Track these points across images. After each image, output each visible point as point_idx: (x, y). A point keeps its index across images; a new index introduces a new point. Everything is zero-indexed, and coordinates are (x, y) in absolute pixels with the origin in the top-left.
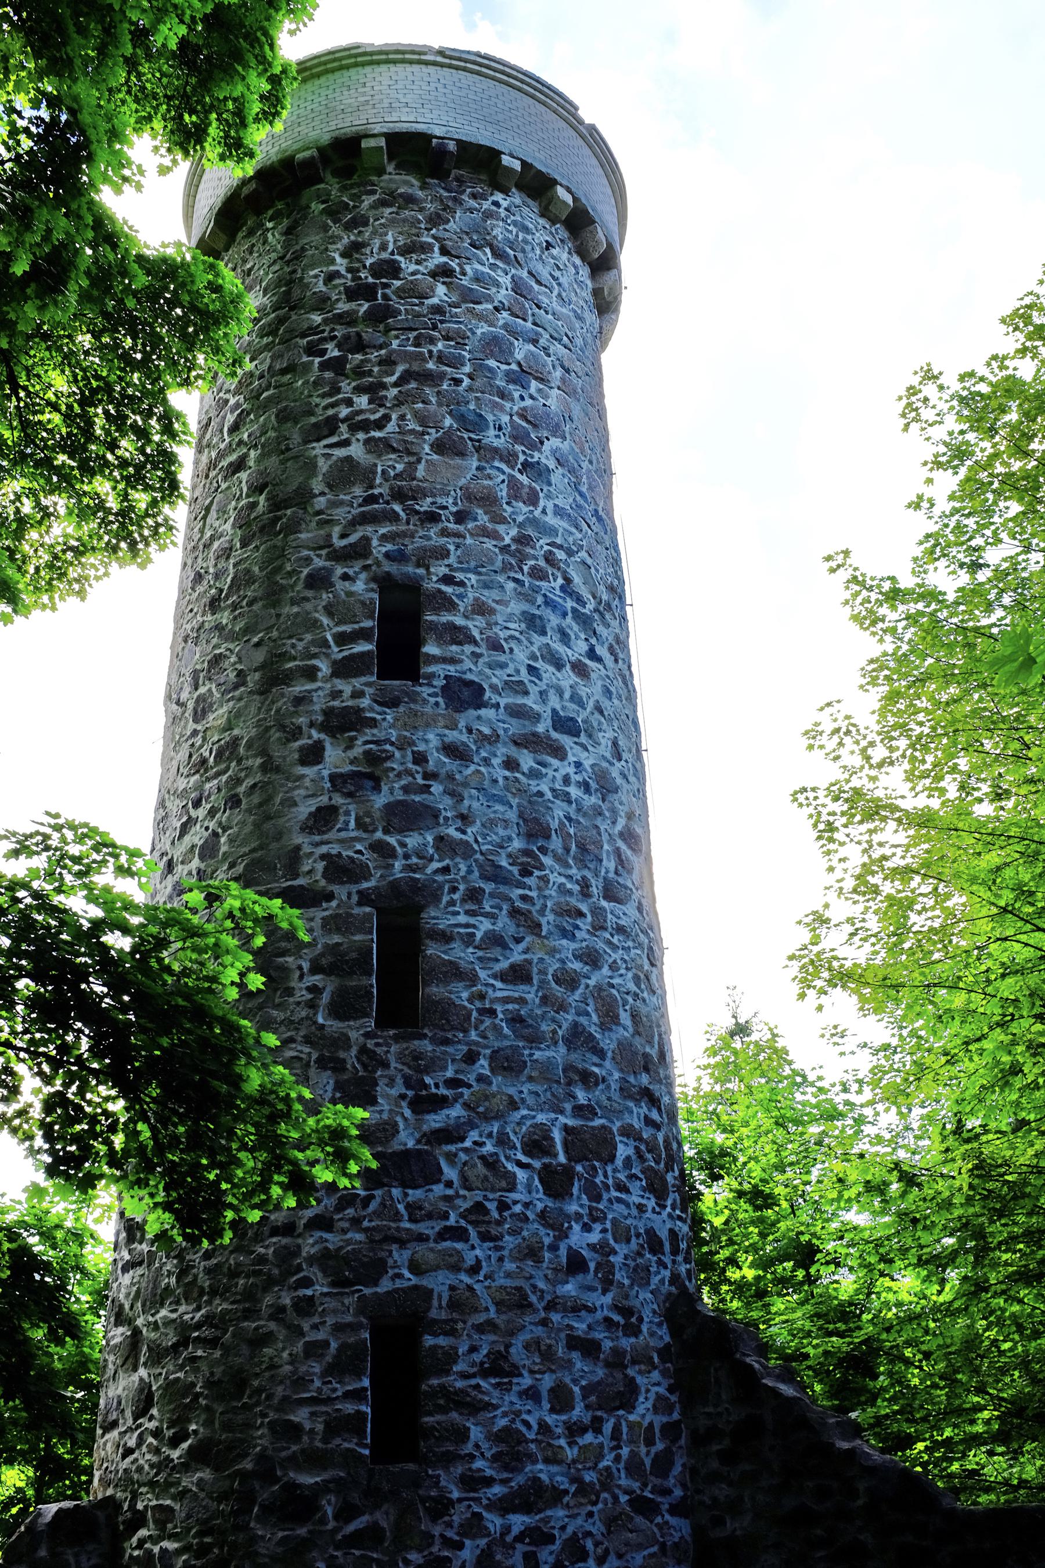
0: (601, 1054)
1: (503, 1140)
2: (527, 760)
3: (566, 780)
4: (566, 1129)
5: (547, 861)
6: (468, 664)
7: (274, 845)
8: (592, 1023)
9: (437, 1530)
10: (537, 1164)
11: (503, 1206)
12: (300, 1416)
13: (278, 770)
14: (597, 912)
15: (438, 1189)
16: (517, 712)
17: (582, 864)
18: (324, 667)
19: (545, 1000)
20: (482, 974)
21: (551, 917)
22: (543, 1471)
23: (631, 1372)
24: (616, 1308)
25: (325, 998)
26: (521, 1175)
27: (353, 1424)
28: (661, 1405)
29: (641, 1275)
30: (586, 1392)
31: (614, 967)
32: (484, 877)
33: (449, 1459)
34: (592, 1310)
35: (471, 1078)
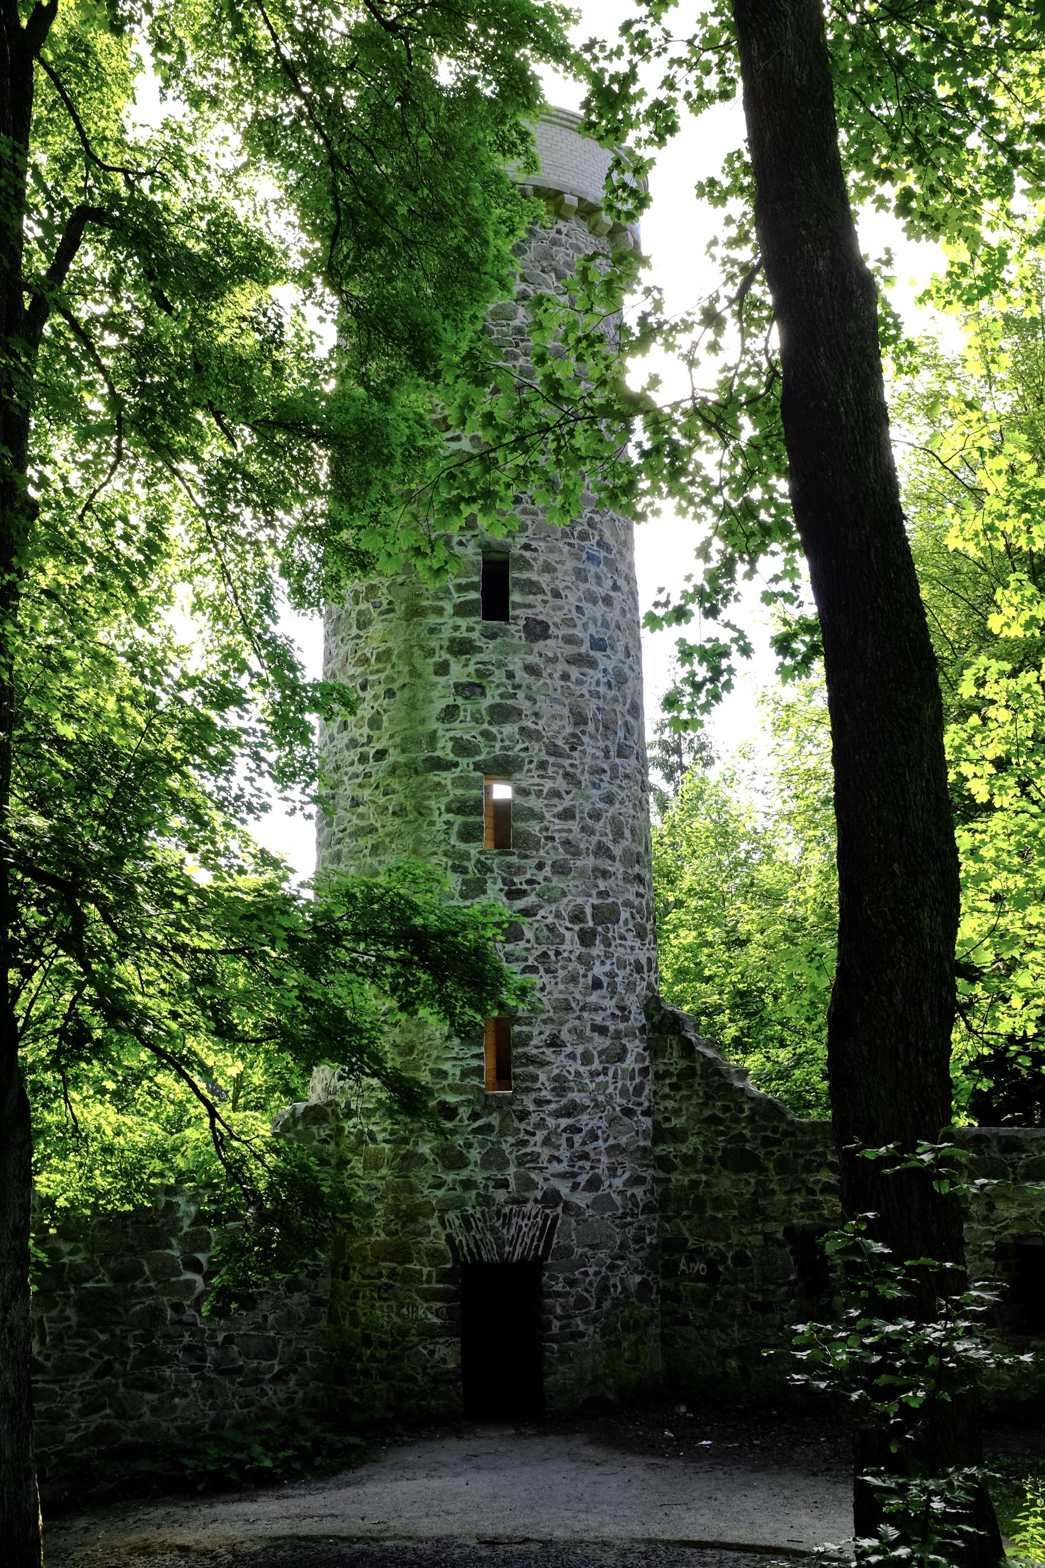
0: (613, 858)
1: (558, 915)
2: (574, 672)
3: (598, 683)
4: (594, 907)
5: (585, 739)
6: (540, 608)
7: (420, 728)
8: (608, 841)
9: (522, 1126)
10: (577, 928)
11: (558, 953)
12: (447, 1066)
13: (420, 676)
14: (614, 768)
15: (523, 944)
16: (570, 640)
17: (605, 737)
18: (449, 609)
19: (583, 829)
20: (547, 815)
21: (587, 776)
22: (577, 1096)
23: (624, 1041)
24: (618, 1007)
25: (456, 828)
26: (568, 935)
27: (478, 1071)
28: (639, 1058)
29: (631, 987)
30: (600, 1053)
31: (622, 802)
32: (549, 753)
33: (528, 1090)
34: (604, 1010)
35: (540, 879)
